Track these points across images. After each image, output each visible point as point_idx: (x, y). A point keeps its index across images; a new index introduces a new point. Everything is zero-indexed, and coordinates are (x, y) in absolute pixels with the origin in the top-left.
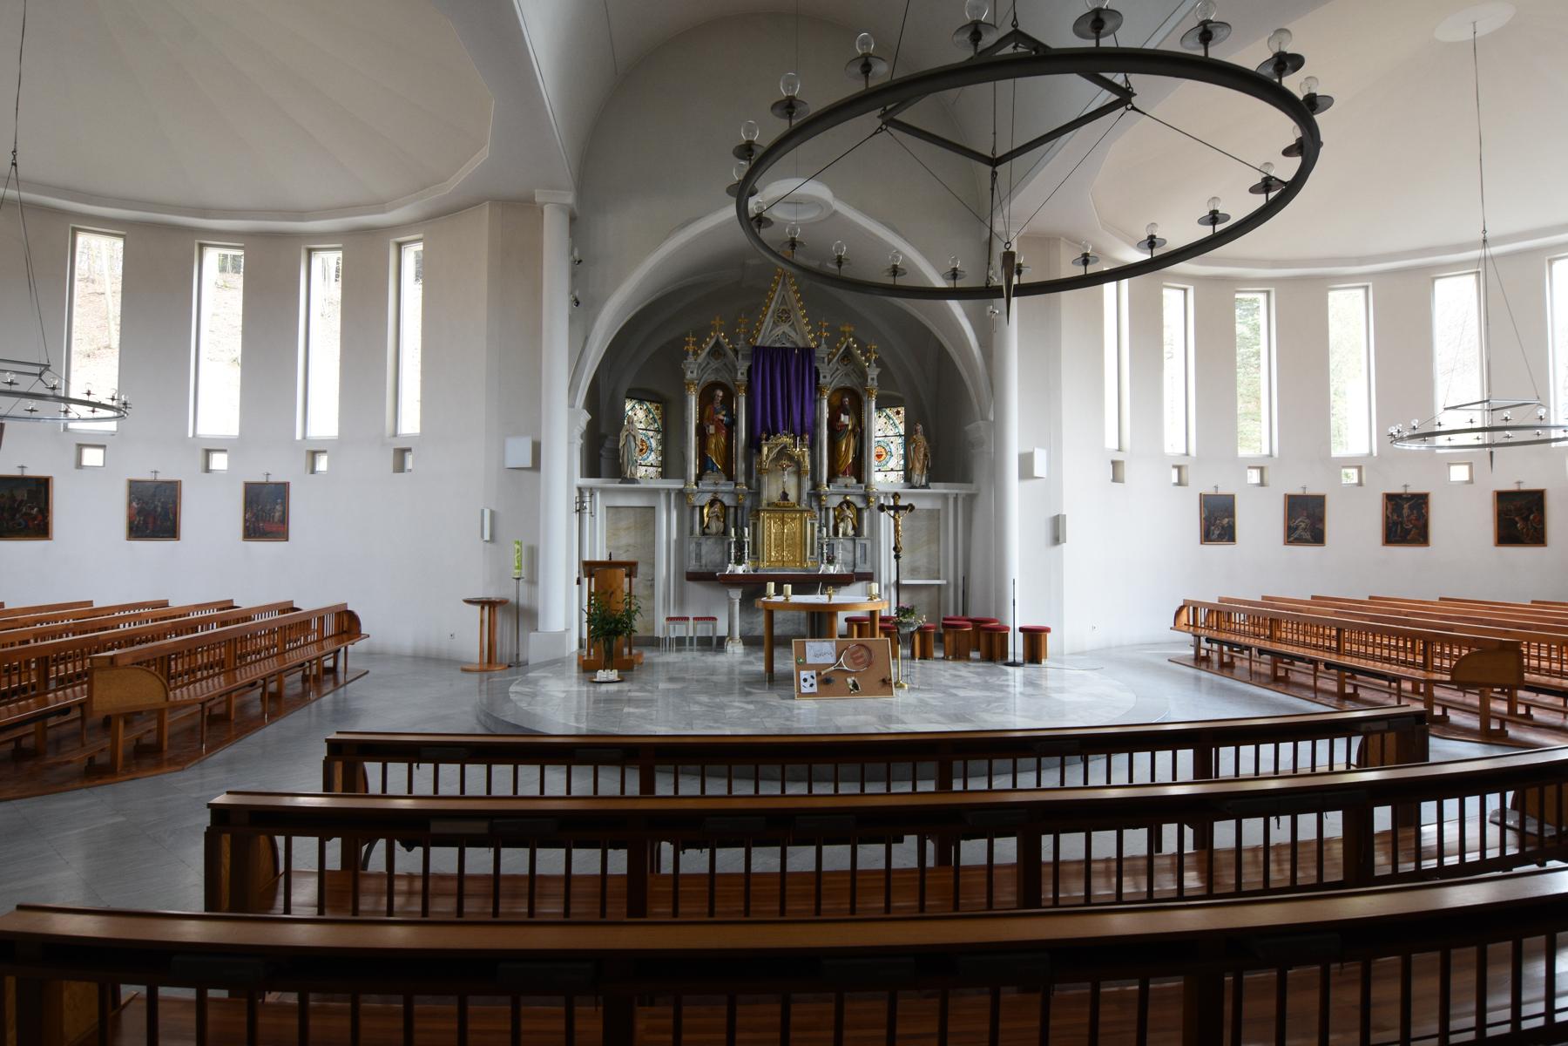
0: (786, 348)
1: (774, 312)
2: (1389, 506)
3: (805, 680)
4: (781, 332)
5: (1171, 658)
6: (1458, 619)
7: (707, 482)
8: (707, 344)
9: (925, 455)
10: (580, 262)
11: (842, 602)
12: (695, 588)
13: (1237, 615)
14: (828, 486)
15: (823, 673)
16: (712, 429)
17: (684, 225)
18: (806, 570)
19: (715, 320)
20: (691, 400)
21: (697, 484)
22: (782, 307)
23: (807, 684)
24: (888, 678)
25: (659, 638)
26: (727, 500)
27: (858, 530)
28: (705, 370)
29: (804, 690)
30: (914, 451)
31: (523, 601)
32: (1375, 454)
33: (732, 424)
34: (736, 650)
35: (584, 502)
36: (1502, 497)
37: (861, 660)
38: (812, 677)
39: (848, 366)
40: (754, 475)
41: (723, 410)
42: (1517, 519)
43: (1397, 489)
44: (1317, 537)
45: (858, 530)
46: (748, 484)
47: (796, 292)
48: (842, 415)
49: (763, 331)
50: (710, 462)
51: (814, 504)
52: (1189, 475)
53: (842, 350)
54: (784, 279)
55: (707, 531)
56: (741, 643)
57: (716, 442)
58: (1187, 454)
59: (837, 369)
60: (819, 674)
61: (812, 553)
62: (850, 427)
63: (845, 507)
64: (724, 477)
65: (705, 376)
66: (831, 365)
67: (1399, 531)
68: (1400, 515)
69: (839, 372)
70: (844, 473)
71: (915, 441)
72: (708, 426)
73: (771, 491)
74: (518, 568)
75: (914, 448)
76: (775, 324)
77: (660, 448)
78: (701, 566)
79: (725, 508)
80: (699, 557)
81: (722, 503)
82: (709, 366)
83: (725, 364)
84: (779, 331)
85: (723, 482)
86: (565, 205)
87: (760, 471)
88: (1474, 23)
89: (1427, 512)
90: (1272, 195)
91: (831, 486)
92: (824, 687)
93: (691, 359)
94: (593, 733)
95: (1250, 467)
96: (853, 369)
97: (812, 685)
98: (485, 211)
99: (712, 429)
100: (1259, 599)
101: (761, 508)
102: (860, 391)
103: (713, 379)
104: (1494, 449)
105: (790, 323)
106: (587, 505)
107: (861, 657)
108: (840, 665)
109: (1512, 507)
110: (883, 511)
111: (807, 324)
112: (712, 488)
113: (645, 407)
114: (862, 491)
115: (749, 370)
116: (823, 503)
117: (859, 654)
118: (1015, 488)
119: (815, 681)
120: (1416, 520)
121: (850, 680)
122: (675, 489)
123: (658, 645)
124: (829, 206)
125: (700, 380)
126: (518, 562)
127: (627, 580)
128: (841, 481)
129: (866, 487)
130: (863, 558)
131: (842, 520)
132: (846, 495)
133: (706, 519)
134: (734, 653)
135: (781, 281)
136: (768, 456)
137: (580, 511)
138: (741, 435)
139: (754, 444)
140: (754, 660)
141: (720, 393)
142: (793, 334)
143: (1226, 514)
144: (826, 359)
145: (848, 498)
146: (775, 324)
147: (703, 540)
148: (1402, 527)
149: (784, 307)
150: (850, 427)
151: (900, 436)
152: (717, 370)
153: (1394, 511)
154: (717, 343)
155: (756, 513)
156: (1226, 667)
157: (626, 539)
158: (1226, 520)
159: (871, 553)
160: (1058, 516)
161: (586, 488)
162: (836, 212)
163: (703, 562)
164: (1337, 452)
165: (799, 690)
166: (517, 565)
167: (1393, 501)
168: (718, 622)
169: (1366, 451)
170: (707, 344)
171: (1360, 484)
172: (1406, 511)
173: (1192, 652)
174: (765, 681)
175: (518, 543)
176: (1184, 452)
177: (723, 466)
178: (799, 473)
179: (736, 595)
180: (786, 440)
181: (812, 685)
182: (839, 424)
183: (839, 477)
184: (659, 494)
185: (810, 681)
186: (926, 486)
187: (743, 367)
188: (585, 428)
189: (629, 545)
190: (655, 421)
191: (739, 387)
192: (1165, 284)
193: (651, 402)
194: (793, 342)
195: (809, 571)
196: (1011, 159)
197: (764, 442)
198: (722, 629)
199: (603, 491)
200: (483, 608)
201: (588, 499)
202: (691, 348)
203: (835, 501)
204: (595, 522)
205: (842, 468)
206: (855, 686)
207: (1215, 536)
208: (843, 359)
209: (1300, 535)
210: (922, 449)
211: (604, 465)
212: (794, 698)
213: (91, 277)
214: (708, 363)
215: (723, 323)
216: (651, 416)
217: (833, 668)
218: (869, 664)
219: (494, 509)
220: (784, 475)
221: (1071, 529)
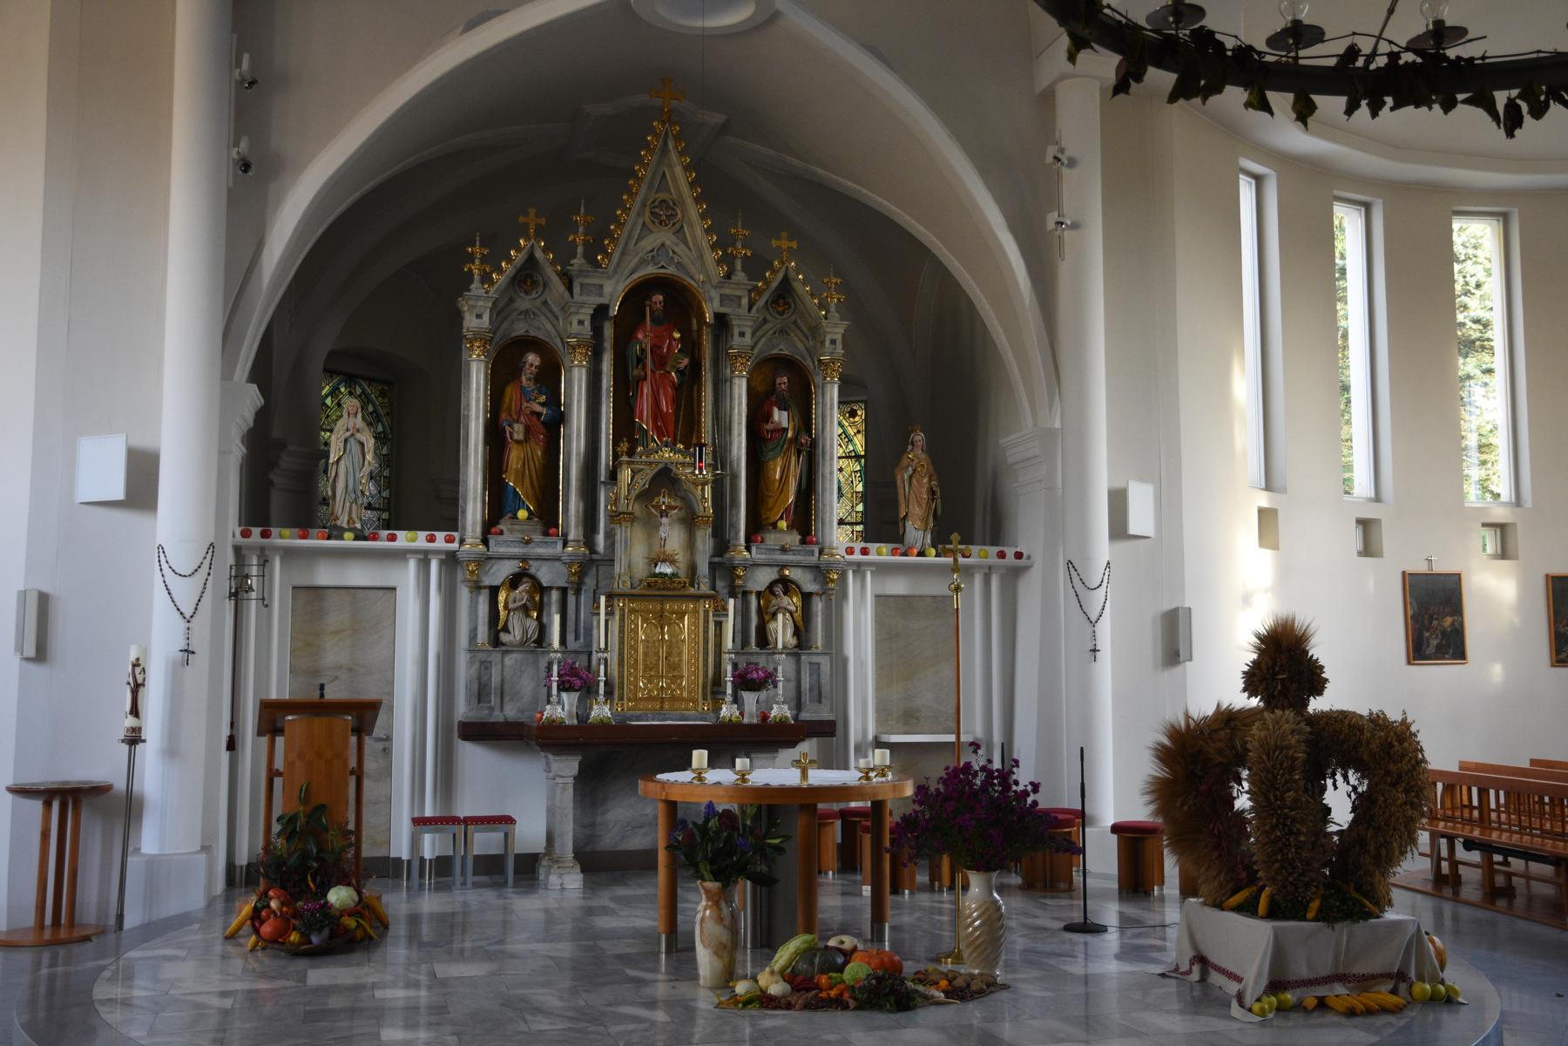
1: (644, 205)
10: (252, 83)
12: (472, 755)
13: (1464, 788)
14: (748, 549)
19: (526, 215)
25: (399, 859)
28: (759, 333)
33: (556, 421)
35: (247, 576)
41: (541, 393)
48: (776, 410)
51: (720, 584)
52: (1388, 538)
55: (504, 637)
56: (578, 869)
59: (765, 321)
62: (790, 435)
63: (779, 589)
64: (539, 528)
69: (767, 327)
75: (911, 477)
77: (386, 473)
79: (540, 589)
81: (533, 577)
85: (537, 537)
91: (754, 549)
93: (476, 288)
99: (518, 431)
100: (1527, 765)
106: (253, 582)
112: (516, 550)
113: (359, 391)
123: (398, 875)
125: (494, 333)
127: (353, 740)
128: (771, 539)
129: (821, 552)
132: (783, 566)
133: (503, 614)
134: (563, 889)
137: (238, 594)
140: (612, 905)
144: (745, 301)
145: (787, 572)
147: (495, 657)
149: (662, 196)
150: (790, 435)
151: (857, 457)
158: (1448, 621)
168: (518, 827)
178: (690, 521)
182: (769, 427)
184: (972, 575)
188: (251, 424)
198: (530, 832)
199: (289, 554)
200: (48, 805)
201: (254, 571)
203: (762, 579)
204: (270, 615)
207: (1431, 650)
211: (277, 500)
213: (1479, 307)
216: (371, 408)
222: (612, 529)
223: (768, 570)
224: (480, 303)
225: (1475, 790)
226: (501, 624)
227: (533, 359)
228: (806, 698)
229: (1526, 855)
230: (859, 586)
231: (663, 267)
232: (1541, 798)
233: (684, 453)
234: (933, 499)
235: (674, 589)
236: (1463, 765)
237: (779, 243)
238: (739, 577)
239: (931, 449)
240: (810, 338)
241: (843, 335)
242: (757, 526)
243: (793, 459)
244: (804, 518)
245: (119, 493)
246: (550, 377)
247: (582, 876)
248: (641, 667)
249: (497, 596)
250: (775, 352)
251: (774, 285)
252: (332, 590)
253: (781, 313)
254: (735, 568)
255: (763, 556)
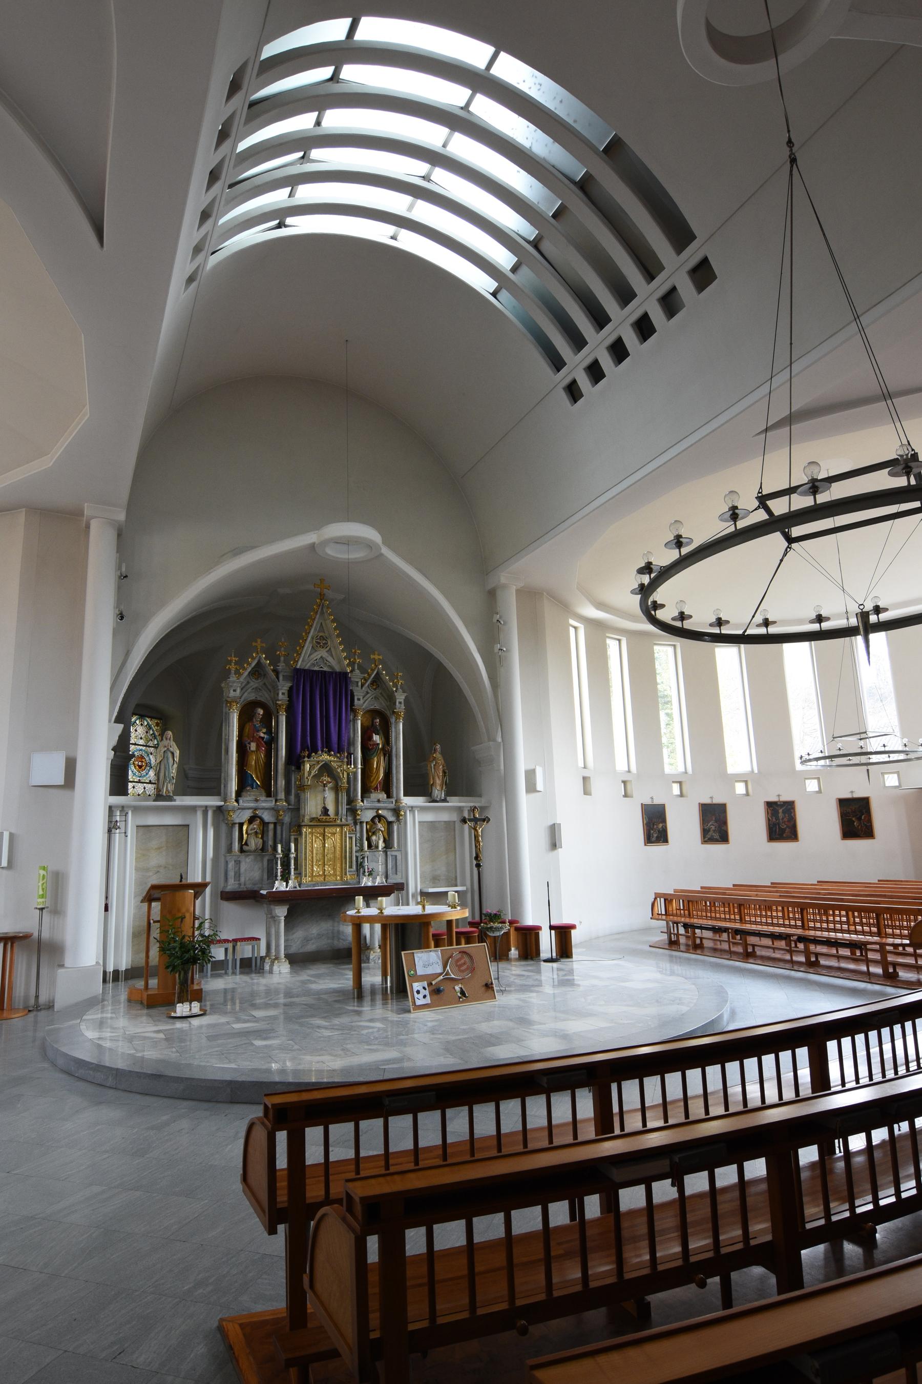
0: (325, 672)
1: (312, 638)
2: (770, 811)
3: (418, 992)
4: (319, 656)
5: (651, 945)
6: (885, 896)
7: (249, 798)
8: (249, 664)
9: (444, 772)
10: (126, 576)
11: (440, 911)
14: (362, 801)
15: (434, 983)
16: (253, 746)
17: (237, 552)
18: (347, 883)
20: (233, 717)
21: (237, 801)
22: (321, 634)
23: (421, 996)
24: (490, 982)
26: (267, 817)
27: (388, 844)
28: (244, 690)
29: (418, 1003)
30: (434, 769)
31: (45, 935)
32: (756, 771)
33: (272, 741)
34: (283, 969)
36: (843, 802)
37: (465, 967)
38: (424, 988)
39: (377, 690)
40: (293, 791)
42: (854, 819)
43: (773, 799)
44: (723, 838)
45: (388, 844)
46: (287, 800)
47: (333, 621)
49: (303, 655)
50: (250, 779)
52: (633, 788)
53: (373, 676)
54: (322, 609)
55: (245, 848)
57: (256, 758)
58: (629, 771)
60: (430, 984)
61: (351, 867)
62: (380, 746)
63: (377, 820)
64: (264, 794)
65: (246, 694)
66: (364, 688)
67: (777, 830)
68: (777, 818)
69: (369, 695)
70: (376, 789)
71: (435, 759)
72: (249, 743)
73: (312, 806)
74: (42, 896)
76: (314, 649)
78: (240, 884)
79: (264, 824)
80: (238, 875)
81: (261, 818)
82: (249, 686)
83: (265, 684)
84: (317, 655)
85: (264, 798)
86: (114, 520)
87: (302, 788)
88: (828, 470)
89: (795, 815)
90: (653, 575)
91: (365, 801)
92: (435, 997)
93: (233, 678)
94: (521, 1061)
95: (673, 782)
96: (381, 694)
97: (425, 997)
98: (21, 517)
99: (253, 746)
101: (303, 824)
102: (388, 713)
103: (254, 698)
104: (870, 767)
105: (328, 648)
107: (464, 964)
108: (447, 974)
109: (850, 810)
110: (465, 822)
111: (343, 651)
112: (252, 805)
113: (146, 723)
114: (392, 806)
115: (290, 690)
116: (358, 817)
117: (463, 961)
118: (524, 800)
119: (427, 992)
120: (788, 821)
121: (457, 988)
122: (212, 807)
124: (378, 548)
126: (43, 889)
128: (374, 796)
129: (396, 801)
130: (394, 869)
131: (374, 833)
133: (245, 836)
134: (280, 973)
135: (320, 610)
136: (310, 772)
138: (282, 753)
139: (295, 762)
141: (261, 711)
142: (330, 659)
143: (660, 820)
144: (360, 684)
145: (380, 812)
146: (314, 649)
147: (242, 857)
148: (779, 826)
150: (380, 746)
152: (257, 689)
153: (772, 815)
154: (259, 664)
155: (297, 827)
156: (697, 947)
157: (156, 859)
158: (661, 825)
159: (398, 865)
160: (554, 824)
161: (117, 807)
162: (382, 555)
163: (242, 879)
164: (731, 770)
165: (414, 1002)
166: (41, 892)
167: (771, 806)
169: (749, 769)
170: (249, 664)
171: (747, 794)
172: (781, 815)
173: (665, 936)
174: (354, 998)
175: (44, 868)
176: (627, 769)
177: (262, 782)
178: (336, 789)
179: (281, 912)
180: (325, 757)
181: (425, 997)
182: (371, 743)
183: (371, 792)
185: (423, 992)
186: (445, 801)
187: (284, 687)
189: (160, 866)
190: (155, 738)
191: (280, 706)
192: (608, 635)
193: (152, 718)
194: (330, 666)
195: (349, 884)
196: (894, 519)
197: (306, 759)
202: (233, 667)
203: (367, 816)
205: (374, 784)
206: (463, 993)
207: (654, 839)
208: (372, 683)
209: (712, 836)
210: (441, 767)
212: (409, 1011)
214: (248, 683)
215: (264, 645)
216: (151, 732)
217: (441, 977)
218: (473, 970)
219: (13, 831)
220: (324, 790)
221: (566, 836)
222: (298, 794)
223: (371, 811)
224: (235, 684)
225: (681, 901)
226: (244, 841)
227: (261, 711)
228: (390, 872)
229: (701, 928)
230: (412, 816)
231: (321, 667)
232: (706, 903)
233: (335, 756)
234: (445, 776)
235: (330, 822)
236: (675, 891)
237: (374, 657)
238: (359, 815)
239: (443, 753)
240: (272, 691)
241: (404, 700)
242: (366, 791)
243: (382, 758)
244: (387, 786)
245: (62, 783)
246: (267, 720)
247: (289, 966)
248: (315, 860)
249: (242, 828)
250: (372, 707)
251: (253, 665)
252: (155, 828)
253: (375, 689)
254: (357, 810)
255: (370, 805)
